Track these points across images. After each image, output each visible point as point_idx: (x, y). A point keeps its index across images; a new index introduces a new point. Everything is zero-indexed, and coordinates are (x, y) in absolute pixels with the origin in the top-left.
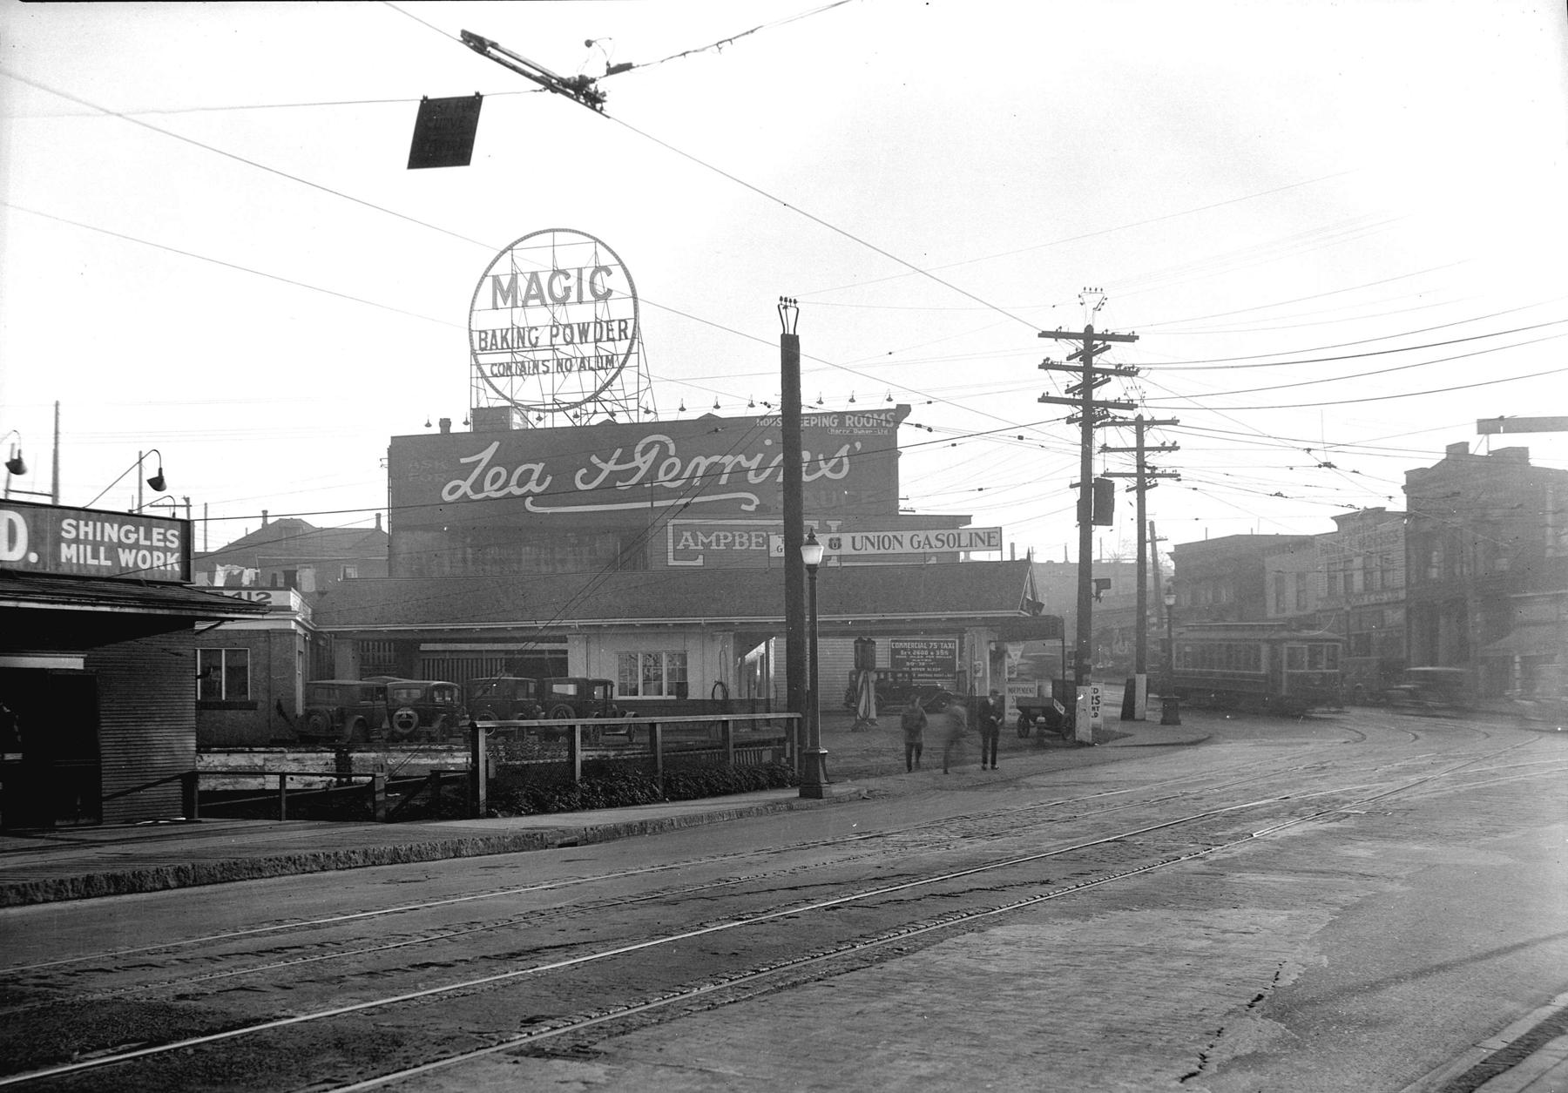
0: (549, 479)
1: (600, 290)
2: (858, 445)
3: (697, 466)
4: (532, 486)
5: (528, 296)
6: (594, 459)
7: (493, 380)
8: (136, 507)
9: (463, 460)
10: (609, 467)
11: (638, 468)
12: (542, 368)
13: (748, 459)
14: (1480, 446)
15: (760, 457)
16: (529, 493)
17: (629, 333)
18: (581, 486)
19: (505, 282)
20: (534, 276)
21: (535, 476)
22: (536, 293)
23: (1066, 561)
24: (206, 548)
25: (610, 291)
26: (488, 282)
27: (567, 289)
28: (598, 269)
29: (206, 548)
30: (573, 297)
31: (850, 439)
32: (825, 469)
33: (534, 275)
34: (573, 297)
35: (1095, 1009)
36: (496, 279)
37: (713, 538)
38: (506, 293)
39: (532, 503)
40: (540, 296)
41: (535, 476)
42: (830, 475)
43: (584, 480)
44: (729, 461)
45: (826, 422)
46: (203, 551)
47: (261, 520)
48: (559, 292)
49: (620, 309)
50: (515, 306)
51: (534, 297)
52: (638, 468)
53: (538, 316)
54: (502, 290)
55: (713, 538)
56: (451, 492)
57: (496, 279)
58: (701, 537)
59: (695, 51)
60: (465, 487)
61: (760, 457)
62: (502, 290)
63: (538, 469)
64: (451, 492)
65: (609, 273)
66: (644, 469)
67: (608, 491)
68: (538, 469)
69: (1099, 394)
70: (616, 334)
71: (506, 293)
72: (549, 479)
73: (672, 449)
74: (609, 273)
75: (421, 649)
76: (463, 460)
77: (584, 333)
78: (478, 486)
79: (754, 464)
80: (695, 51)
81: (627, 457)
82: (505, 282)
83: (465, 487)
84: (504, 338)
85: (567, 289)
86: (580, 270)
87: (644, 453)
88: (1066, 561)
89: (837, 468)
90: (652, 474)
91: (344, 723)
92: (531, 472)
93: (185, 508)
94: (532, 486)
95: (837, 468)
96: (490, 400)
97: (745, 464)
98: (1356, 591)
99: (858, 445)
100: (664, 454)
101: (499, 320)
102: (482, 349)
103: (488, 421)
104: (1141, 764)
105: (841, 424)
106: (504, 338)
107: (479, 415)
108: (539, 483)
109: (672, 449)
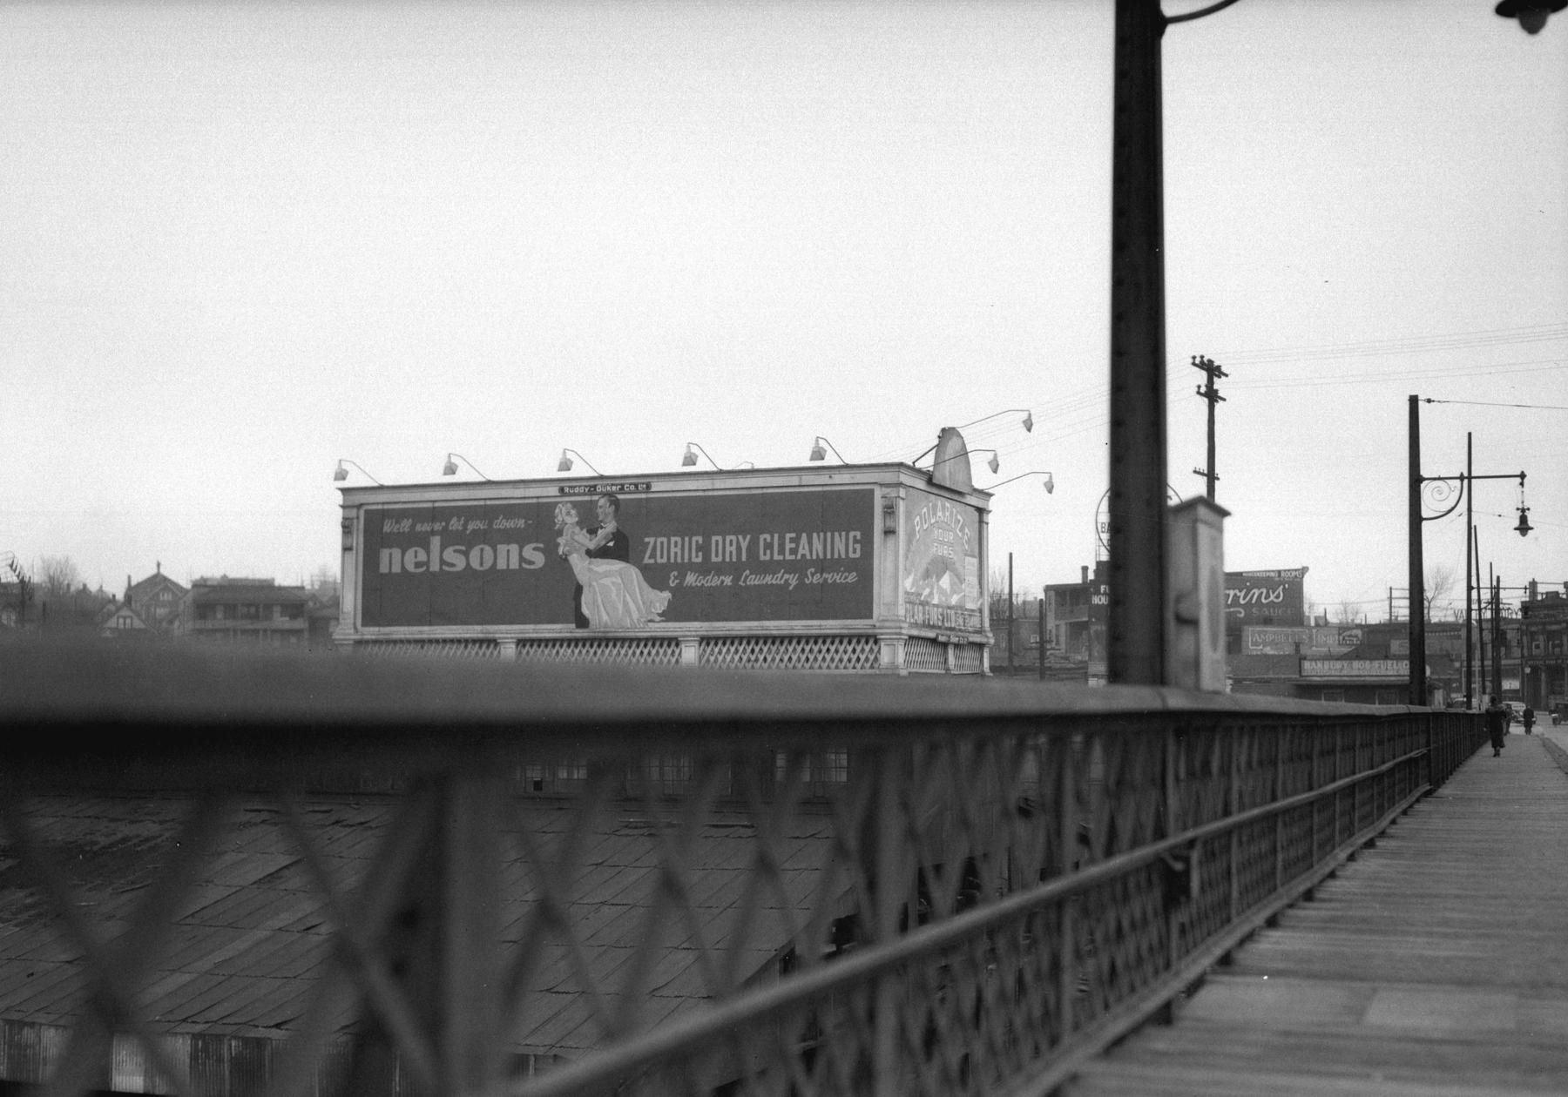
2: (1287, 586)
3: (1254, 594)
8: (150, 1088)
13: (1240, 591)
23: (390, 572)
24: (508, 565)
29: (508, 565)
31: (1282, 583)
42: (1276, 600)
45: (1272, 574)
46: (505, 567)
58: (1262, 636)
59: (1439, 402)
61: (1245, 590)
69: (951, 651)
80: (1439, 402)
88: (390, 572)
89: (1277, 597)
93: (1473, 475)
95: (1277, 597)
97: (1238, 594)
98: (1441, 691)
99: (1287, 586)
104: (1387, 1078)
105: (1280, 576)
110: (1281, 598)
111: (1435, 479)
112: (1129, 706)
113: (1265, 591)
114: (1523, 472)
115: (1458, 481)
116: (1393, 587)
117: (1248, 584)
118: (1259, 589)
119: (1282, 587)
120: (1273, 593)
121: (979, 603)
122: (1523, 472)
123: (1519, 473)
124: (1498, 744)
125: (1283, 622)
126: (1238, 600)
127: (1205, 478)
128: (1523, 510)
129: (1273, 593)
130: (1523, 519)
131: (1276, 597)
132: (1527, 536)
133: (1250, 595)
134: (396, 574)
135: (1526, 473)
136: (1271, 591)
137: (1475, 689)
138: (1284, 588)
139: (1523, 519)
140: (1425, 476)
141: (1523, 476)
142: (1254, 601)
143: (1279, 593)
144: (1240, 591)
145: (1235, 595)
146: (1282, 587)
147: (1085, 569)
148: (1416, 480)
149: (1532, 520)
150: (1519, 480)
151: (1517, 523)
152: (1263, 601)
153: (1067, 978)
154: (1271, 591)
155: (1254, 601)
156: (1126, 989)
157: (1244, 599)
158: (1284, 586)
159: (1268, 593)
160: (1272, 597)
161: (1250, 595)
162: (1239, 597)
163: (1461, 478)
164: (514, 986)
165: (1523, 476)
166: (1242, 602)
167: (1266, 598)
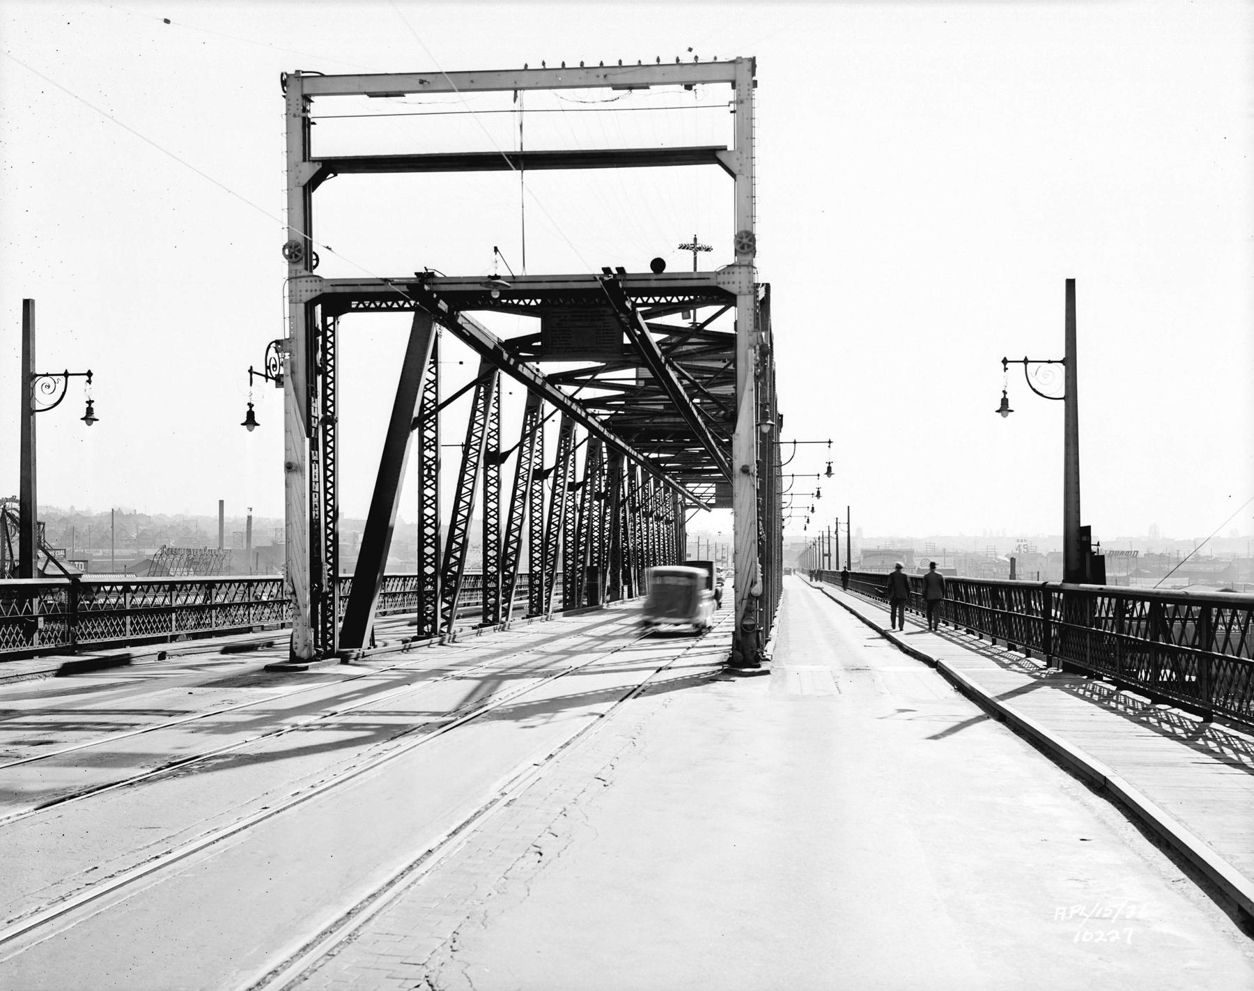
24: (522, 149)
29: (522, 149)
111: (44, 375)
114: (89, 371)
115: (1023, 363)
121: (715, 625)
122: (89, 371)
123: (86, 372)
124: (1045, 583)
127: (697, 310)
130: (90, 411)
132: (253, 431)
139: (90, 411)
141: (89, 374)
148: (29, 378)
150: (87, 378)
156: (152, 525)
163: (1026, 364)
164: (216, 597)
165: (89, 374)
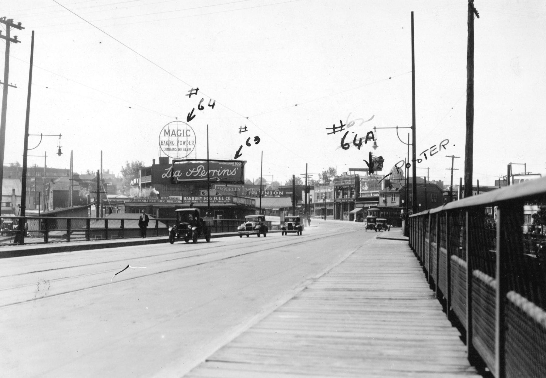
0: (181, 174)
1: (188, 135)
2: (237, 168)
3: (224, 171)
4: (178, 175)
5: (172, 135)
6: (190, 170)
7: (164, 151)
9: (166, 170)
10: (192, 172)
11: (197, 172)
12: (175, 150)
13: (218, 171)
14: (349, 173)
15: (220, 170)
16: (178, 177)
17: (194, 144)
18: (187, 176)
19: (167, 131)
20: (174, 130)
21: (179, 173)
22: (174, 134)
25: (190, 135)
26: (163, 131)
27: (181, 134)
28: (187, 130)
30: (182, 135)
32: (231, 173)
33: (174, 130)
34: (182, 135)
35: (337, 299)
36: (165, 131)
37: (223, 189)
38: (167, 133)
39: (179, 179)
40: (175, 134)
41: (179, 173)
43: (188, 174)
44: (214, 171)
47: (83, 179)
48: (179, 135)
49: (190, 139)
50: (169, 136)
51: (174, 135)
52: (197, 172)
53: (174, 139)
54: (166, 133)
55: (223, 189)
56: (164, 176)
57: (165, 131)
60: (166, 175)
61: (220, 170)
62: (166, 133)
63: (179, 171)
64: (164, 176)
65: (190, 131)
66: (199, 172)
67: (192, 177)
68: (179, 171)
70: (191, 144)
71: (167, 133)
72: (181, 174)
73: (204, 169)
74: (190, 131)
75: (258, 231)
76: (166, 170)
77: (184, 143)
78: (168, 175)
79: (219, 172)
81: (195, 170)
82: (167, 131)
83: (166, 175)
84: (167, 143)
85: (181, 134)
86: (184, 130)
87: (199, 169)
90: (200, 173)
91: (92, 224)
92: (178, 172)
94: (178, 175)
95: (234, 173)
96: (163, 155)
97: (217, 172)
99: (237, 168)
100: (202, 169)
101: (166, 138)
102: (162, 145)
103: (164, 161)
106: (167, 143)
107: (161, 159)
108: (180, 174)
109: (204, 169)
110: (235, 174)
112: (117, 227)
113: (228, 170)
116: (512, 163)
117: (221, 167)
118: (226, 170)
119: (235, 169)
120: (232, 171)
122: (240, 133)
125: (237, 183)
126: (217, 174)
128: (60, 147)
129: (232, 171)
130: (60, 150)
131: (233, 173)
132: (61, 156)
133: (222, 172)
134: (157, 165)
135: (239, 133)
136: (231, 171)
137: (37, 199)
138: (236, 170)
139: (60, 150)
140: (410, 129)
141: (60, 136)
142: (223, 175)
143: (234, 172)
144: (218, 171)
145: (216, 172)
146: (235, 169)
147: (154, 160)
149: (62, 152)
151: (58, 151)
152: (228, 175)
153: (485, 314)
154: (231, 171)
155: (223, 175)
157: (219, 174)
158: (237, 169)
159: (229, 171)
160: (231, 173)
161: (222, 172)
162: (217, 173)
166: (218, 175)
167: (228, 174)
